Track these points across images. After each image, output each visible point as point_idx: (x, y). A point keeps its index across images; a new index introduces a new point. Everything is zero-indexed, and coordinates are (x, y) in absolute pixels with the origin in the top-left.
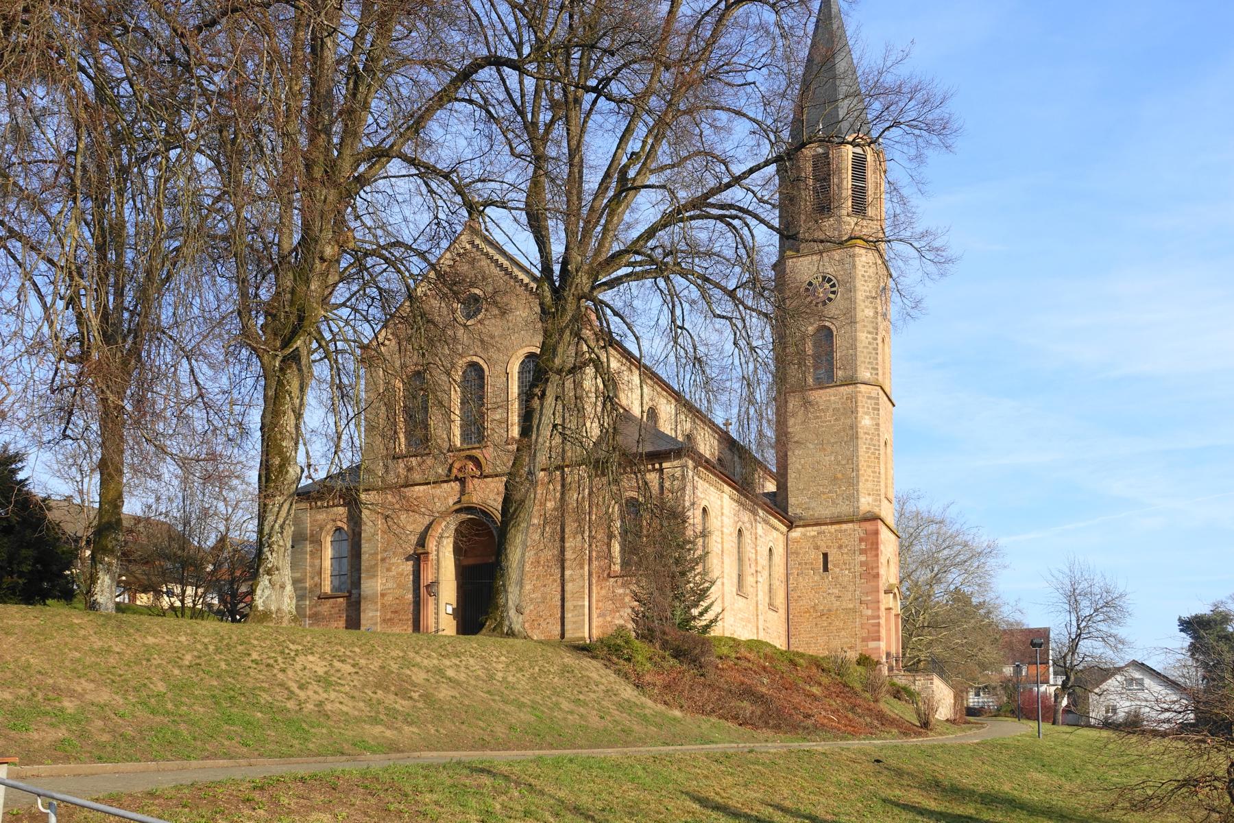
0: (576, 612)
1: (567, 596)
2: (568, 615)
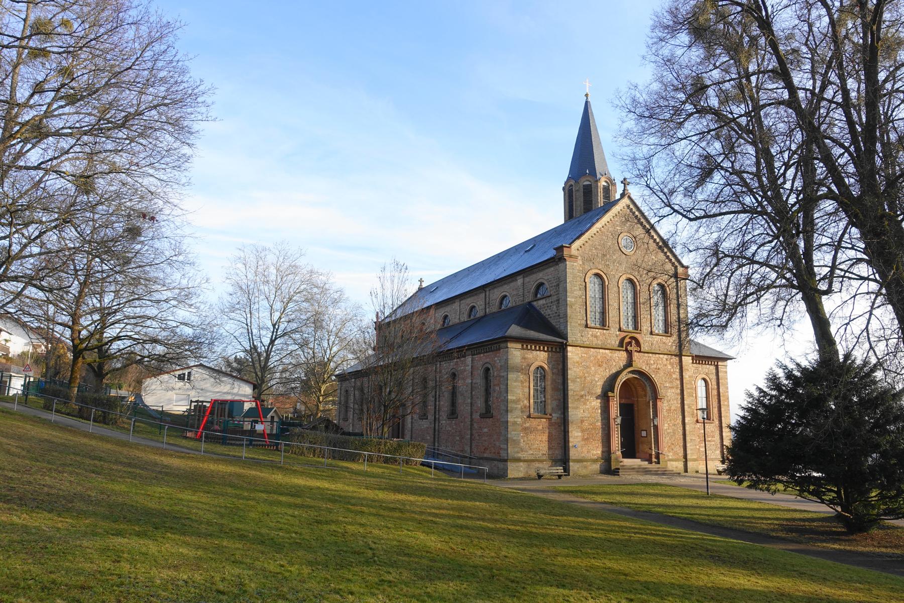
1: (687, 432)
2: (688, 445)
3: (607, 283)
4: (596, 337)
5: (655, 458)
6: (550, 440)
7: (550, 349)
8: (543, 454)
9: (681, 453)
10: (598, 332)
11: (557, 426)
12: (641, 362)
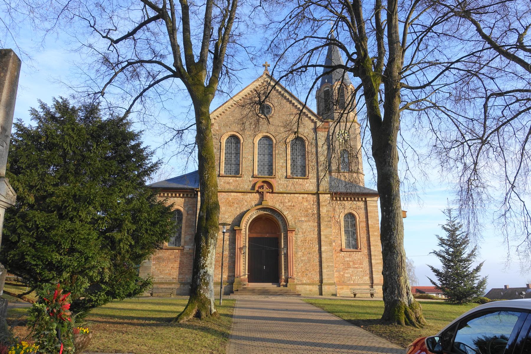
0: (329, 269)
1: (324, 260)
2: (324, 271)
3: (242, 141)
4: (228, 183)
5: (285, 282)
6: (181, 267)
7: (185, 195)
8: (173, 278)
9: (317, 278)
10: (231, 180)
11: (188, 256)
12: (271, 201)
